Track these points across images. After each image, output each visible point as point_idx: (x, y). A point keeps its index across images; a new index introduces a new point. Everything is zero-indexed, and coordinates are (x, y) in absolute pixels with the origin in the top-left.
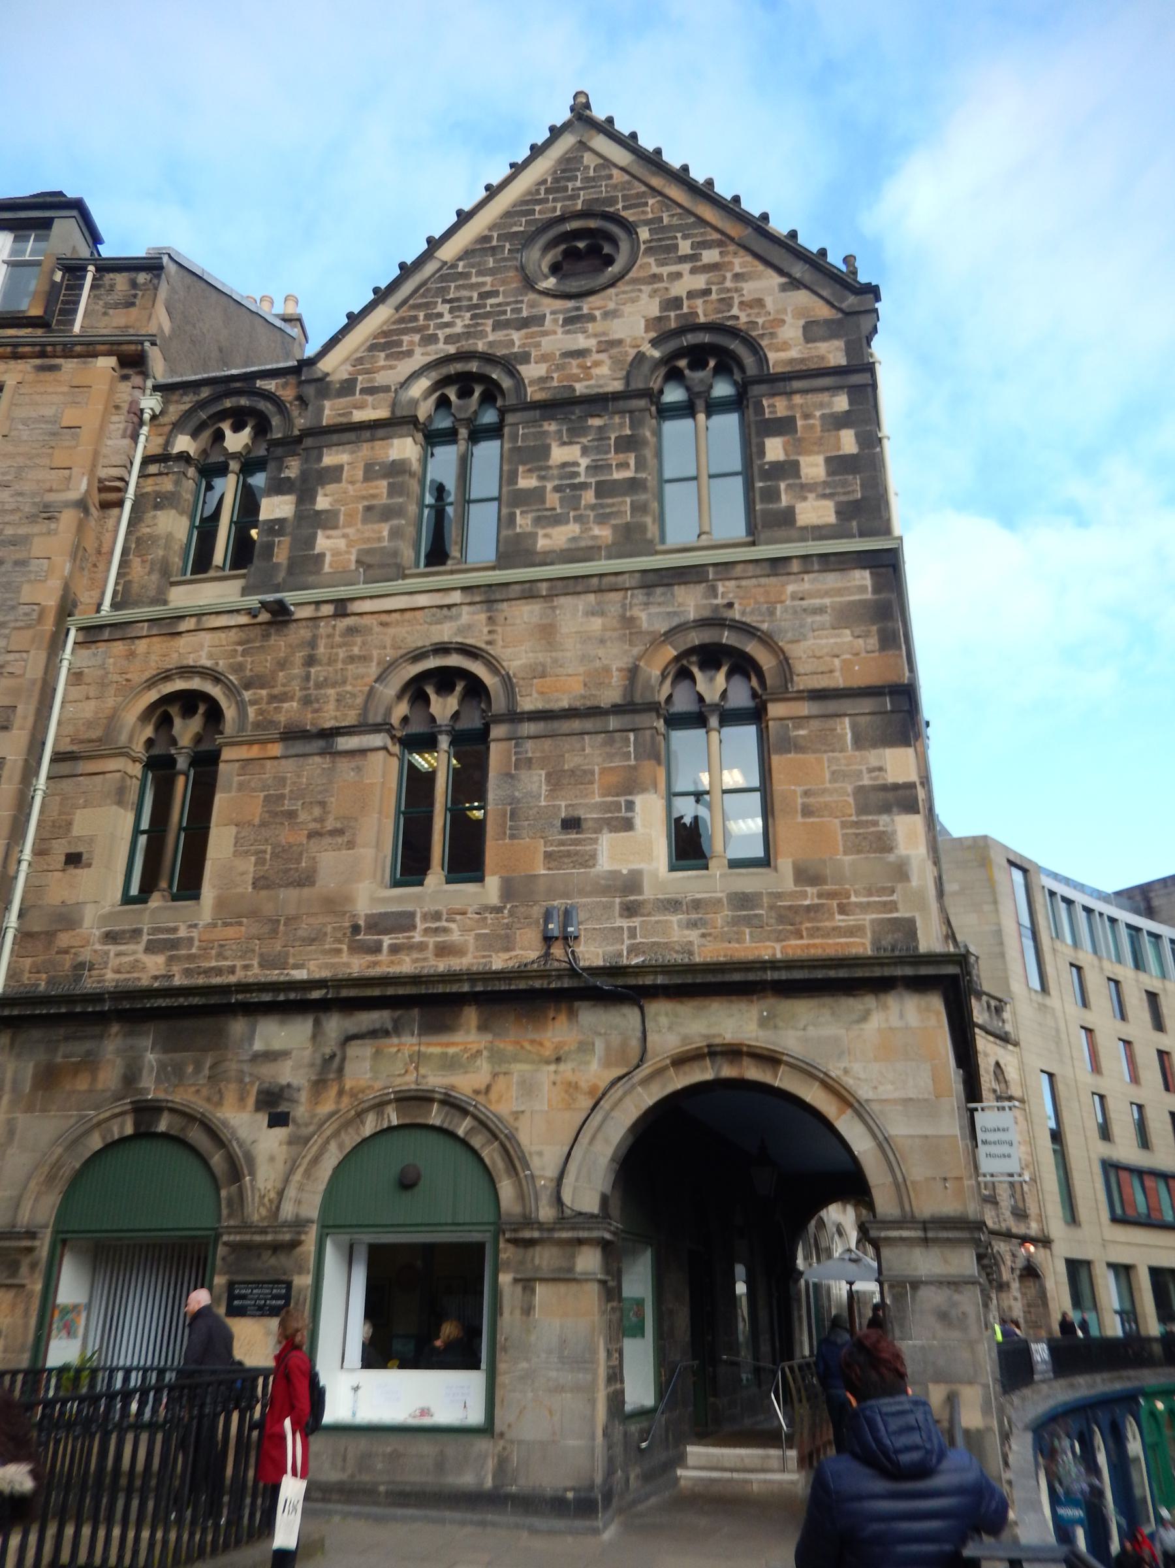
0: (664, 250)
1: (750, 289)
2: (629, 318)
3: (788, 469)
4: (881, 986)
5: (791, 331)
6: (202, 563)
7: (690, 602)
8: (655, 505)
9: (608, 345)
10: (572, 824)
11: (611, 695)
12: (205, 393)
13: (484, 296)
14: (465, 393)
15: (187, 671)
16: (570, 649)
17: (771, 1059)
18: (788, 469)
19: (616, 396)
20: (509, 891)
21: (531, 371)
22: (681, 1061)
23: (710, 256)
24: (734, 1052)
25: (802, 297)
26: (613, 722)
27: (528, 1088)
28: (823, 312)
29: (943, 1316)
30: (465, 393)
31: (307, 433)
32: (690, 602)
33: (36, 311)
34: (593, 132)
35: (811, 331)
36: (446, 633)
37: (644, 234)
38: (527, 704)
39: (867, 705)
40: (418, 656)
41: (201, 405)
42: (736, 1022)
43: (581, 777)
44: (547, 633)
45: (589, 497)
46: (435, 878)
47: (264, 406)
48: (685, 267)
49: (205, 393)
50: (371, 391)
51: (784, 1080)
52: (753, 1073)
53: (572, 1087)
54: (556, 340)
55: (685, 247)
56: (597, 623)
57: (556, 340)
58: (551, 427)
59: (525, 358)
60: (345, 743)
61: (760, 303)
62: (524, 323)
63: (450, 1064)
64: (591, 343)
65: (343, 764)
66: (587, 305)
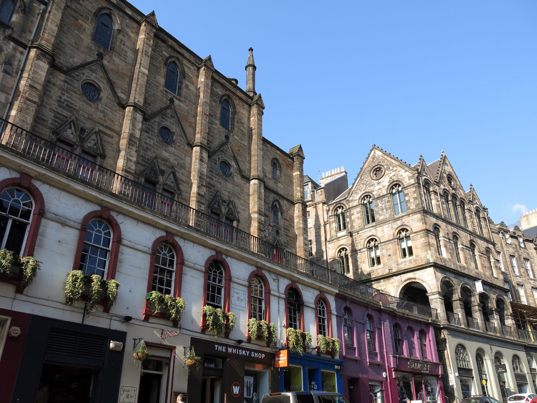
0: (388, 169)
1: (401, 173)
2: (385, 181)
3: (409, 201)
4: (426, 267)
5: (407, 179)
6: (340, 230)
7: (399, 223)
8: (247, 210)
9: (384, 186)
10: (390, 255)
11: (392, 238)
12: (334, 205)
13: (367, 182)
14: (367, 198)
15: (341, 245)
16: (386, 232)
17: (415, 279)
18: (409, 201)
19: (386, 195)
20: (384, 265)
21: (374, 193)
22: (405, 281)
23: (395, 169)
24: (411, 279)
25: (407, 173)
26: (392, 241)
27: (390, 287)
28: (411, 175)
29: (435, 302)
30: (367, 198)
31: (349, 209)
32: (399, 223)
33: (311, 199)
34: (56, 71)
35: (410, 178)
36: (371, 234)
37: (385, 167)
38: (382, 241)
39: (422, 232)
40: (368, 237)
41: (334, 207)
42: (410, 275)
43: (390, 249)
44: (383, 231)
45: (385, 211)
46: (376, 265)
47: (342, 205)
48: (392, 171)
49: (334, 205)
50: (355, 200)
51: (417, 281)
52: (413, 280)
53: (394, 286)
54: (377, 187)
55: (391, 168)
56: (388, 229)
57: (377, 187)
58: (378, 201)
59: (373, 191)
60: (362, 251)
61: (402, 175)
62: (372, 185)
63: (381, 286)
64: (381, 187)
65: (363, 253)
66: (380, 180)
